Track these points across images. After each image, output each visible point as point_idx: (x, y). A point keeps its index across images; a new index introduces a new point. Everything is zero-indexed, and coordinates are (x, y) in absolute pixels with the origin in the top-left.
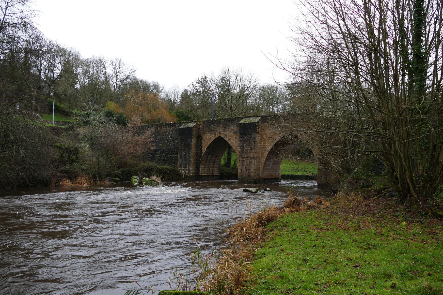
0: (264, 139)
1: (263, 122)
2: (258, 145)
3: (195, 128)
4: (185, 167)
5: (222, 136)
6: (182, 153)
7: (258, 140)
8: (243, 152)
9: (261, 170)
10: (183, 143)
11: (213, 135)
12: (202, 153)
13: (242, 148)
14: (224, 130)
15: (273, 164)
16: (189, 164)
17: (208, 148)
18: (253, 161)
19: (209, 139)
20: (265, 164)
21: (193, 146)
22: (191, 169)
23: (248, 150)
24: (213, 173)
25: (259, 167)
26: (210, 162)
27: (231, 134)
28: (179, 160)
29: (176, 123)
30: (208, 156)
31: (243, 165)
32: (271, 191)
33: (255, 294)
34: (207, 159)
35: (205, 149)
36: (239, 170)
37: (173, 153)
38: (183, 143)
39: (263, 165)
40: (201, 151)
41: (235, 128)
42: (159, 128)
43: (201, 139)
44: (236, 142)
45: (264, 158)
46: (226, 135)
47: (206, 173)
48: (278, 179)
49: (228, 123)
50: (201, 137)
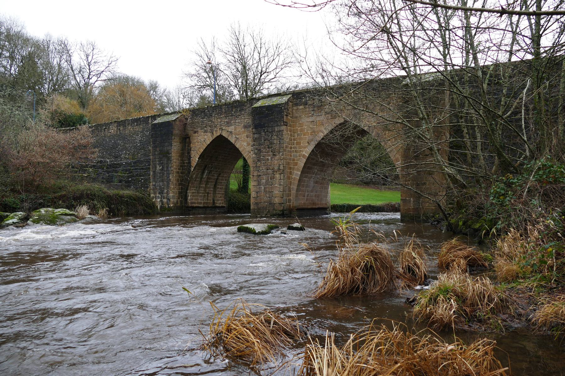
0: (298, 135)
1: (296, 105)
2: (287, 147)
3: (177, 123)
4: (161, 193)
5: (225, 134)
6: (156, 167)
7: (286, 136)
8: (258, 161)
9: (294, 192)
10: (158, 149)
11: (209, 134)
12: (190, 166)
13: (258, 152)
14: (228, 123)
15: (316, 182)
16: (168, 187)
17: (202, 157)
18: (277, 176)
19: (202, 141)
20: (300, 180)
21: (173, 154)
22: (171, 195)
23: (269, 155)
24: (214, 203)
25: (289, 188)
26: (207, 183)
27: (240, 129)
28: (151, 180)
29: (149, 117)
30: (203, 173)
31: (259, 184)
32: (301, 229)
33: (388, 6)
34: (202, 178)
35: (195, 159)
36: (253, 194)
37: (143, 169)
38: (158, 149)
39: (297, 182)
40: (190, 163)
41: (246, 119)
42: (121, 129)
43: (190, 143)
44: (248, 144)
45: (298, 170)
46: (231, 132)
47: (201, 203)
48: (324, 210)
49: (234, 110)
50: (189, 138)
